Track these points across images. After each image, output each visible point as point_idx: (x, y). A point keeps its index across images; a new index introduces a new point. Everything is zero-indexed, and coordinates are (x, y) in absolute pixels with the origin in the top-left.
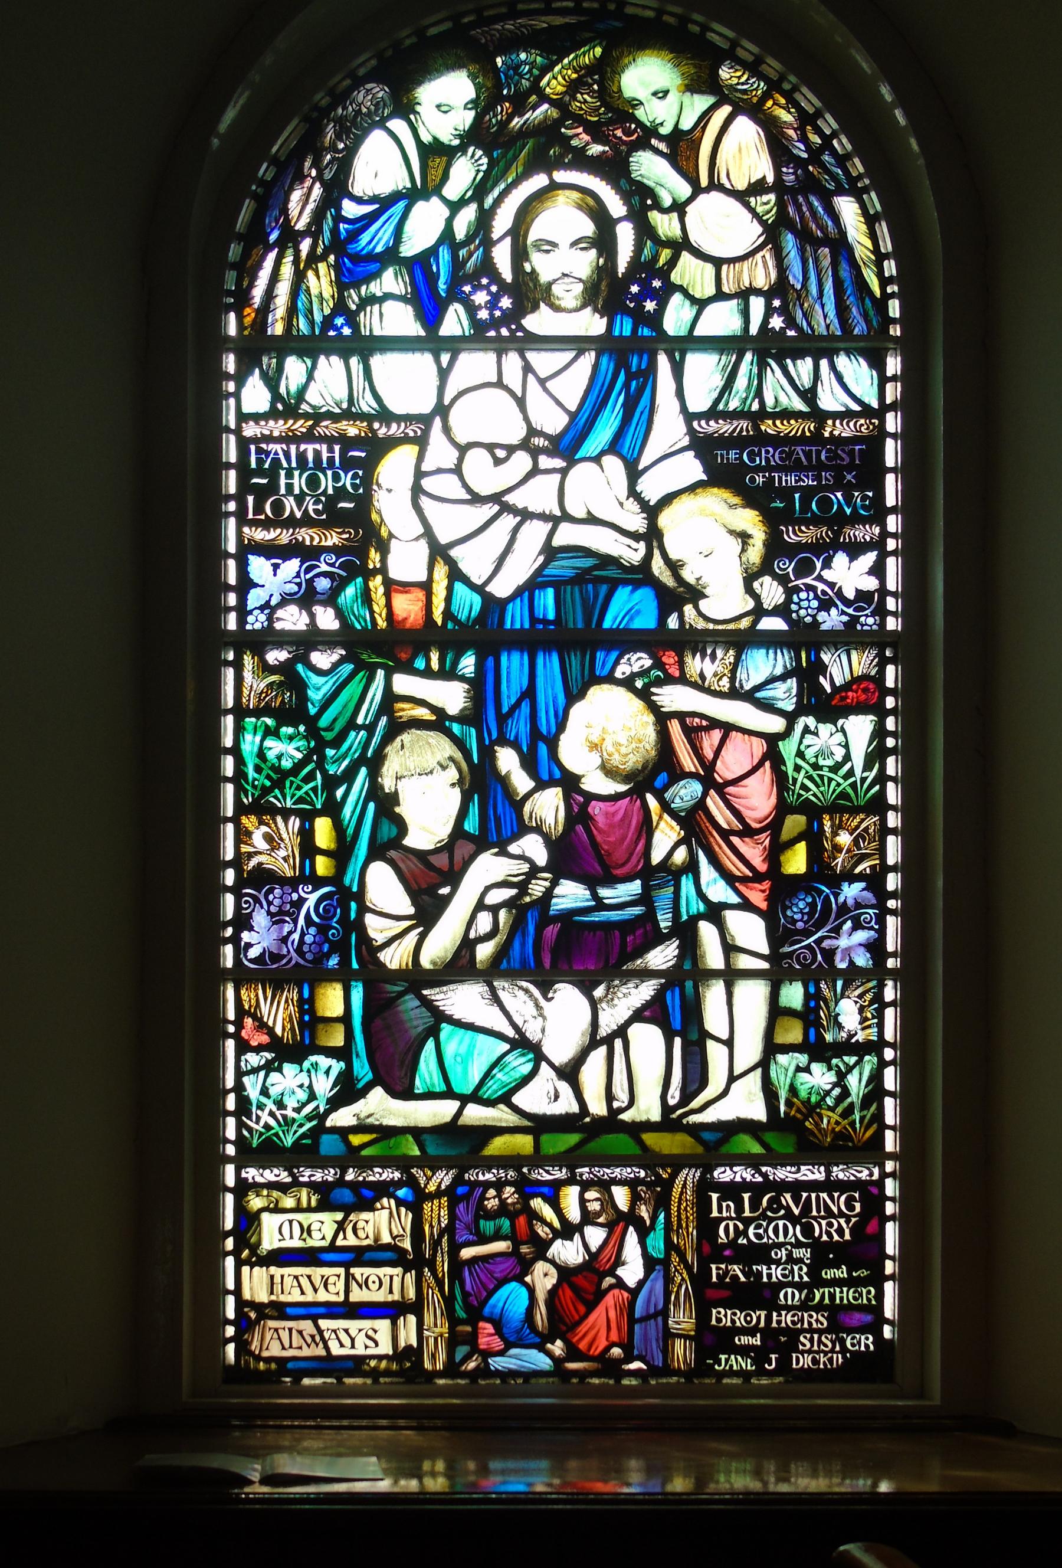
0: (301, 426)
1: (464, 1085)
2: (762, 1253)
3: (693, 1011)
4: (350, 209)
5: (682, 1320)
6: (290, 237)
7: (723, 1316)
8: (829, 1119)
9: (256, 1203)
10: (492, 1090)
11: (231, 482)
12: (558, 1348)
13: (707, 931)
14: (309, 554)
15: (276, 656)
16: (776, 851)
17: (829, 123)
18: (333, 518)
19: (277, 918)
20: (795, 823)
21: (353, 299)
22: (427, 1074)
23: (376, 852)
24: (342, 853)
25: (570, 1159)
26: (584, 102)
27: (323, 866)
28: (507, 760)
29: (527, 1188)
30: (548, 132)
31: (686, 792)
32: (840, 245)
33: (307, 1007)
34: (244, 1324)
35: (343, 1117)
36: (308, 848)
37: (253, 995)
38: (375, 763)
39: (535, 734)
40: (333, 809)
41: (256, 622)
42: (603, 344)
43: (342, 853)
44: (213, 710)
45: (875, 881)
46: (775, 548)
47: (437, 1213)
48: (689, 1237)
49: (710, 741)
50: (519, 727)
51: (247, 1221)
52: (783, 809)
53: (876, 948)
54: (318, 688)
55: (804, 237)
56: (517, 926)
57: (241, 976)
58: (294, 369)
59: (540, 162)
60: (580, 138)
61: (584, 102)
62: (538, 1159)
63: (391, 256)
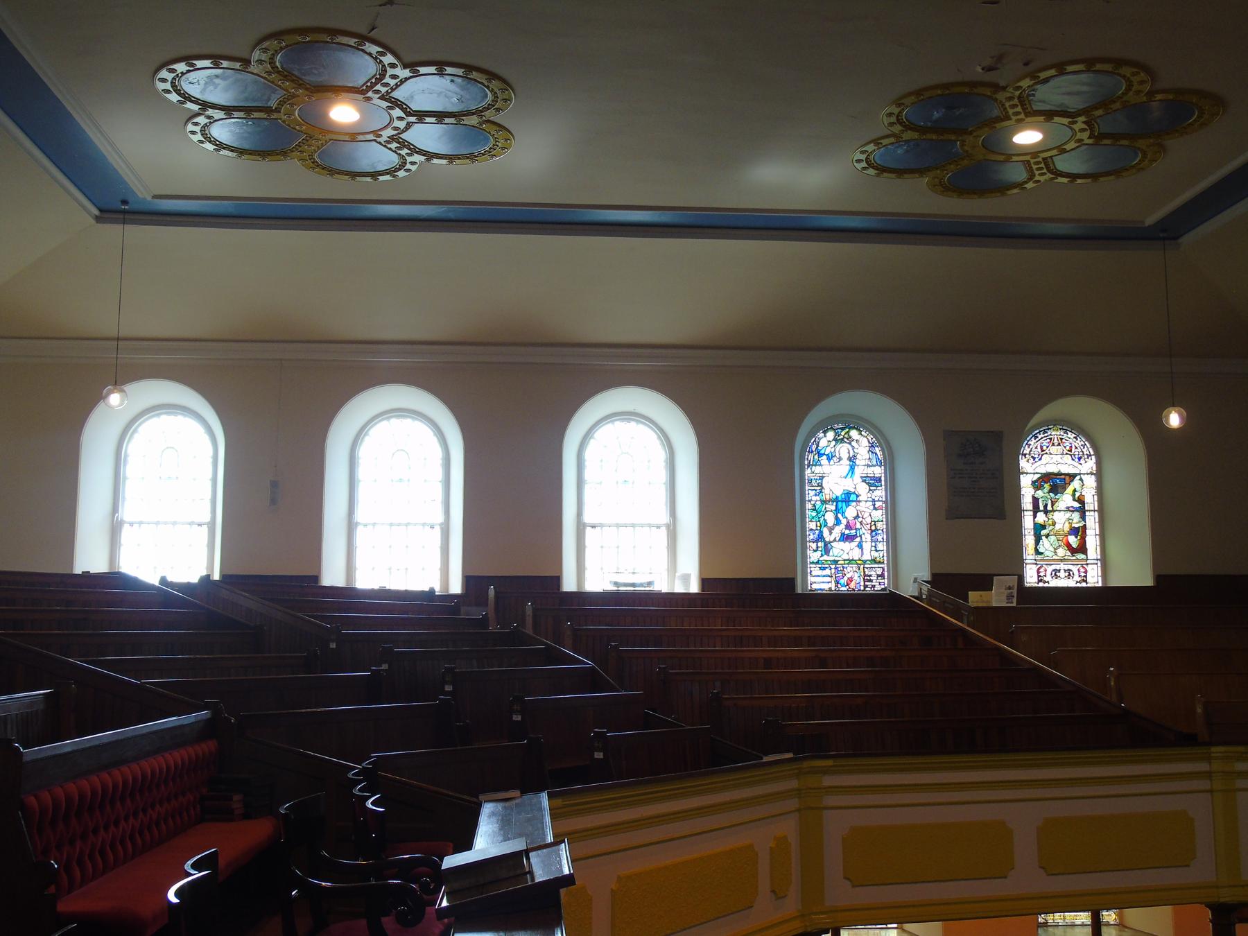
0: (814, 475)
1: (835, 555)
2: (871, 576)
3: (862, 546)
4: (819, 448)
5: (862, 583)
6: (812, 452)
7: (867, 583)
8: (878, 559)
9: (812, 569)
10: (839, 555)
11: (807, 481)
12: (847, 587)
13: (863, 536)
14: (816, 490)
15: (813, 503)
16: (871, 526)
17: (874, 439)
18: (818, 486)
19: (814, 534)
20: (873, 523)
21: (820, 459)
22: (831, 554)
23: (824, 526)
24: (821, 527)
25: (848, 564)
26: (846, 436)
27: (819, 528)
28: (840, 516)
29: (843, 567)
30: (842, 440)
31: (860, 519)
32: (876, 454)
33: (817, 545)
34: (811, 584)
35: (821, 559)
36: (817, 526)
37: (811, 544)
38: (824, 516)
39: (843, 512)
40: (819, 521)
41: (810, 498)
42: (850, 465)
43: (821, 527)
44: (864, 592)
45: (882, 530)
46: (870, 490)
47: (833, 571)
48: (862, 574)
49: (863, 513)
50: (841, 511)
51: (811, 571)
52: (872, 521)
53: (883, 539)
54: (817, 507)
55: (872, 452)
56: (841, 536)
57: (810, 542)
58: (814, 467)
59: (841, 443)
60: (846, 440)
61: (846, 436)
62: (844, 564)
63: (824, 454)
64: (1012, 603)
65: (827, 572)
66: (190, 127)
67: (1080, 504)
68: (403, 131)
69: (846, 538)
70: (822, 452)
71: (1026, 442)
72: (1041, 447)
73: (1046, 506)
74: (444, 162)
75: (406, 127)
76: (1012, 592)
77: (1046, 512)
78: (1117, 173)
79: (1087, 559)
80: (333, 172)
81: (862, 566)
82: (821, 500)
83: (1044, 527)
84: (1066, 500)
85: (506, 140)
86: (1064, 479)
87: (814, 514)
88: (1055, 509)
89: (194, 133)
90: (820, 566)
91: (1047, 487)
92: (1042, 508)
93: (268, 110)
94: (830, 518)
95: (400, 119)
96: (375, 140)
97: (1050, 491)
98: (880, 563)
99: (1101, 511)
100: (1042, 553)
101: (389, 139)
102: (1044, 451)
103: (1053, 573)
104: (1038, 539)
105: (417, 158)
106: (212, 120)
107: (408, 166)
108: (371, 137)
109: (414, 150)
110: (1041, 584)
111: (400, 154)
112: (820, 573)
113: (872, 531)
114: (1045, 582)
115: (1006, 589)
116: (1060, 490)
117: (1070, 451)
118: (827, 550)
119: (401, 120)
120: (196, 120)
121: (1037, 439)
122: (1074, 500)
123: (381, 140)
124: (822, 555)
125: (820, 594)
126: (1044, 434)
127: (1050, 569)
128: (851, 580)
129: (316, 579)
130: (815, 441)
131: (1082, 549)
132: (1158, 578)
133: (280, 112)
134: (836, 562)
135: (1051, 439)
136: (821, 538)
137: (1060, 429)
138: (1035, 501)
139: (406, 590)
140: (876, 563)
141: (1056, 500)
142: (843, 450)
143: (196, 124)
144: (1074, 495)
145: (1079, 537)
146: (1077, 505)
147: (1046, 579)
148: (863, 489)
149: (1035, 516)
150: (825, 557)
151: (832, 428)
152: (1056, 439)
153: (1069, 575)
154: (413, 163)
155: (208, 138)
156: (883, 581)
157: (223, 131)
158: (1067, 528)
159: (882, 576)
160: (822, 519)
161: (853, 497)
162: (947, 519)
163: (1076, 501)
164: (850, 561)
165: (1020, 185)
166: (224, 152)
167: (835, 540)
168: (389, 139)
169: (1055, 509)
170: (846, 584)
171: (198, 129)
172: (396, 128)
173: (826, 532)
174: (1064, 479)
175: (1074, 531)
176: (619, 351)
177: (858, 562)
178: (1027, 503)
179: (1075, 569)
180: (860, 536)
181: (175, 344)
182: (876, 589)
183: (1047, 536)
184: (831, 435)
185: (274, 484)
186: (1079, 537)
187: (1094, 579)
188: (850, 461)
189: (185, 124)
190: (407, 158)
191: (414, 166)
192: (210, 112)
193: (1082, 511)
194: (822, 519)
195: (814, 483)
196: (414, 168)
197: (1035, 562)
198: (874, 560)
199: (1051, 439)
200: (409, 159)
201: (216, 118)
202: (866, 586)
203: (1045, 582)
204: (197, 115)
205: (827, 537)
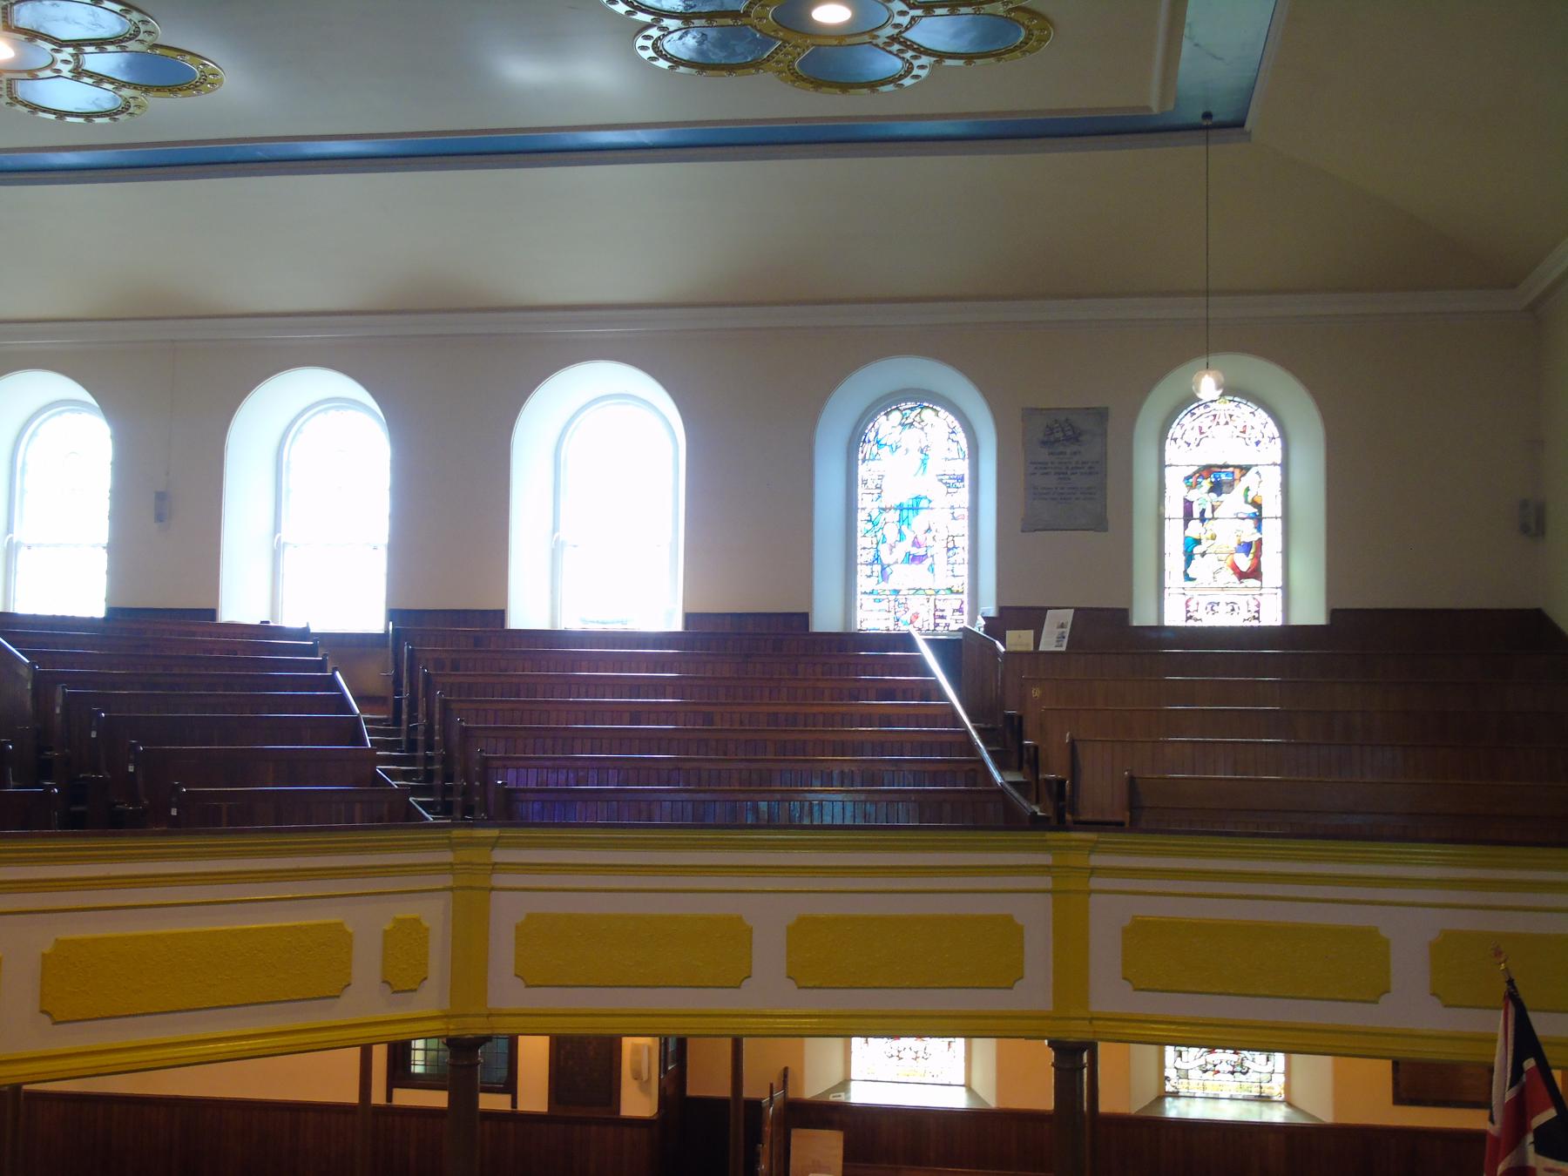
4: (879, 437)
7: (938, 621)
21: (879, 452)
23: (883, 543)
24: (878, 544)
26: (918, 419)
30: (912, 424)
43: (878, 544)
47: (892, 603)
64: (1061, 646)
65: (884, 605)
66: (640, 42)
67: (1254, 507)
68: (907, 29)
69: (915, 559)
70: (882, 442)
71: (1177, 421)
72: (1200, 428)
73: (1203, 512)
74: (960, 63)
75: (910, 22)
76: (1063, 632)
77: (1203, 519)
78: (997, 55)
79: (1261, 588)
80: (845, 87)
81: (932, 598)
82: (879, 508)
83: (1198, 542)
84: (1233, 502)
85: (1042, 30)
86: (1233, 473)
87: (870, 525)
88: (1215, 516)
89: (644, 48)
90: (875, 597)
91: (1206, 484)
92: (1196, 514)
93: (735, 14)
94: (891, 532)
95: (903, 13)
96: (870, 42)
97: (1211, 490)
98: (958, 592)
99: (1286, 517)
100: (1194, 579)
101: (887, 40)
102: (1203, 433)
103: (1209, 607)
104: (1189, 557)
105: (925, 60)
106: (667, 32)
107: (916, 72)
108: (866, 38)
109: (921, 51)
110: (1191, 623)
111: (903, 58)
112: (877, 606)
113: (949, 550)
114: (1196, 620)
115: (1058, 628)
116: (1224, 489)
117: (1244, 432)
118: (884, 576)
119: (904, 15)
120: (646, 33)
121: (1195, 417)
122: (1246, 502)
123: (880, 41)
124: (878, 583)
125: (874, 634)
126: (1205, 408)
127: (1204, 601)
128: (916, 616)
129: (212, 613)
130: (873, 426)
131: (1255, 573)
132: (1334, 614)
133: (750, 16)
134: (897, 592)
135: (1215, 416)
136: (877, 559)
137: (1230, 401)
138: (1188, 506)
139: (35, 615)
140: (952, 592)
141: (1218, 503)
142: (912, 438)
143: (648, 37)
144: (1246, 496)
145: (1251, 556)
146: (1252, 510)
147: (1196, 615)
148: (937, 492)
149: (1186, 526)
150: (883, 585)
151: (897, 408)
152: (1222, 416)
153: (1233, 610)
154: (922, 67)
155: (660, 53)
156: (961, 617)
157: (682, 44)
158: (1234, 544)
159: (960, 610)
160: (879, 534)
161: (924, 503)
162: (1023, 531)
163: (1250, 504)
164: (917, 590)
165: (895, 79)
166: (682, 69)
167: (896, 563)
168: (887, 40)
169: (1215, 516)
170: (909, 622)
171: (649, 43)
172: (897, 26)
173: (884, 549)
174: (1233, 473)
175: (1246, 547)
176: (603, 313)
177: (929, 592)
178: (1174, 508)
179: (1241, 602)
180: (932, 556)
181: (47, 325)
182: (950, 629)
183: (1203, 554)
184: (896, 416)
185: (161, 497)
186: (1251, 556)
187: (1272, 617)
188: (922, 452)
189: (635, 36)
190: (913, 61)
191: (924, 71)
192: (666, 22)
193: (1258, 519)
194: (879, 534)
195: (871, 485)
196: (924, 73)
197: (1183, 591)
198: (950, 589)
199: (1215, 416)
200: (916, 63)
201: (671, 29)
202: (937, 625)
203: (1196, 620)
204: (649, 26)
205: (886, 558)
